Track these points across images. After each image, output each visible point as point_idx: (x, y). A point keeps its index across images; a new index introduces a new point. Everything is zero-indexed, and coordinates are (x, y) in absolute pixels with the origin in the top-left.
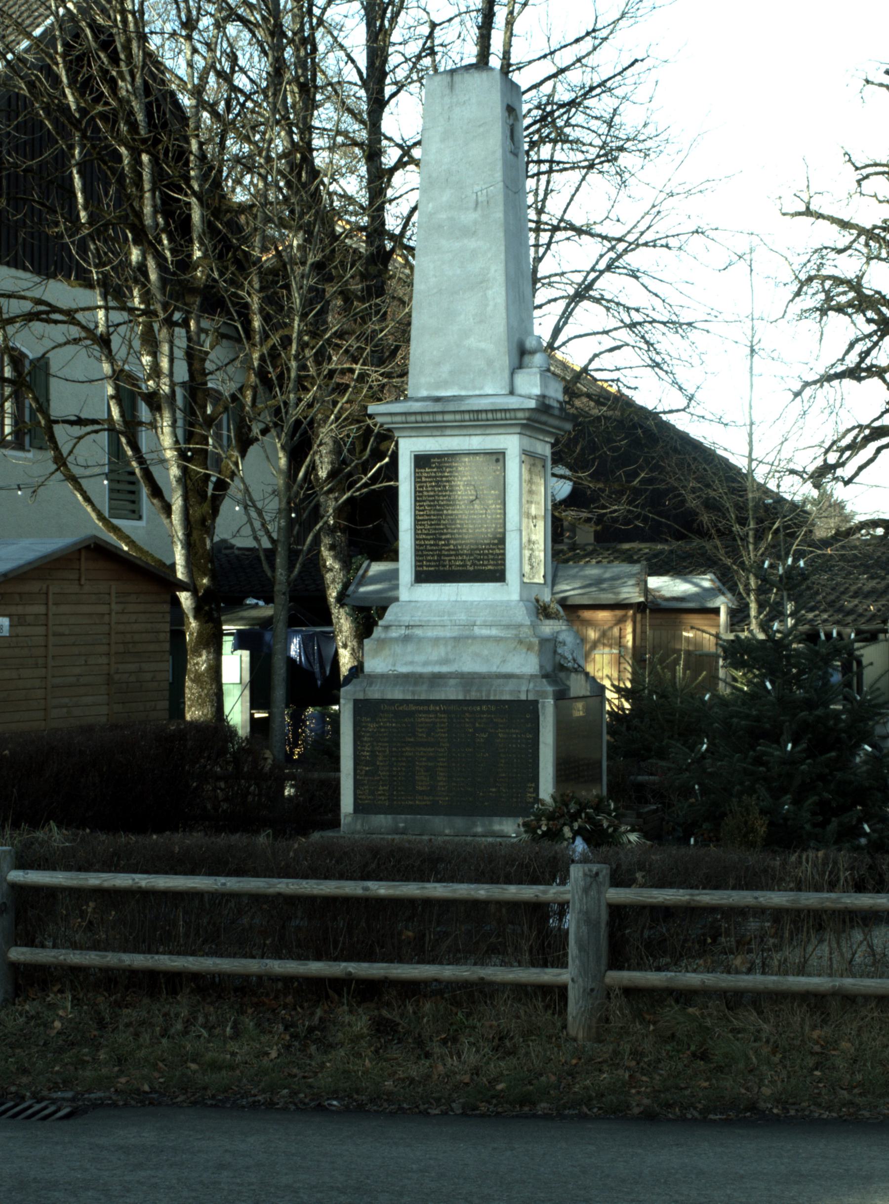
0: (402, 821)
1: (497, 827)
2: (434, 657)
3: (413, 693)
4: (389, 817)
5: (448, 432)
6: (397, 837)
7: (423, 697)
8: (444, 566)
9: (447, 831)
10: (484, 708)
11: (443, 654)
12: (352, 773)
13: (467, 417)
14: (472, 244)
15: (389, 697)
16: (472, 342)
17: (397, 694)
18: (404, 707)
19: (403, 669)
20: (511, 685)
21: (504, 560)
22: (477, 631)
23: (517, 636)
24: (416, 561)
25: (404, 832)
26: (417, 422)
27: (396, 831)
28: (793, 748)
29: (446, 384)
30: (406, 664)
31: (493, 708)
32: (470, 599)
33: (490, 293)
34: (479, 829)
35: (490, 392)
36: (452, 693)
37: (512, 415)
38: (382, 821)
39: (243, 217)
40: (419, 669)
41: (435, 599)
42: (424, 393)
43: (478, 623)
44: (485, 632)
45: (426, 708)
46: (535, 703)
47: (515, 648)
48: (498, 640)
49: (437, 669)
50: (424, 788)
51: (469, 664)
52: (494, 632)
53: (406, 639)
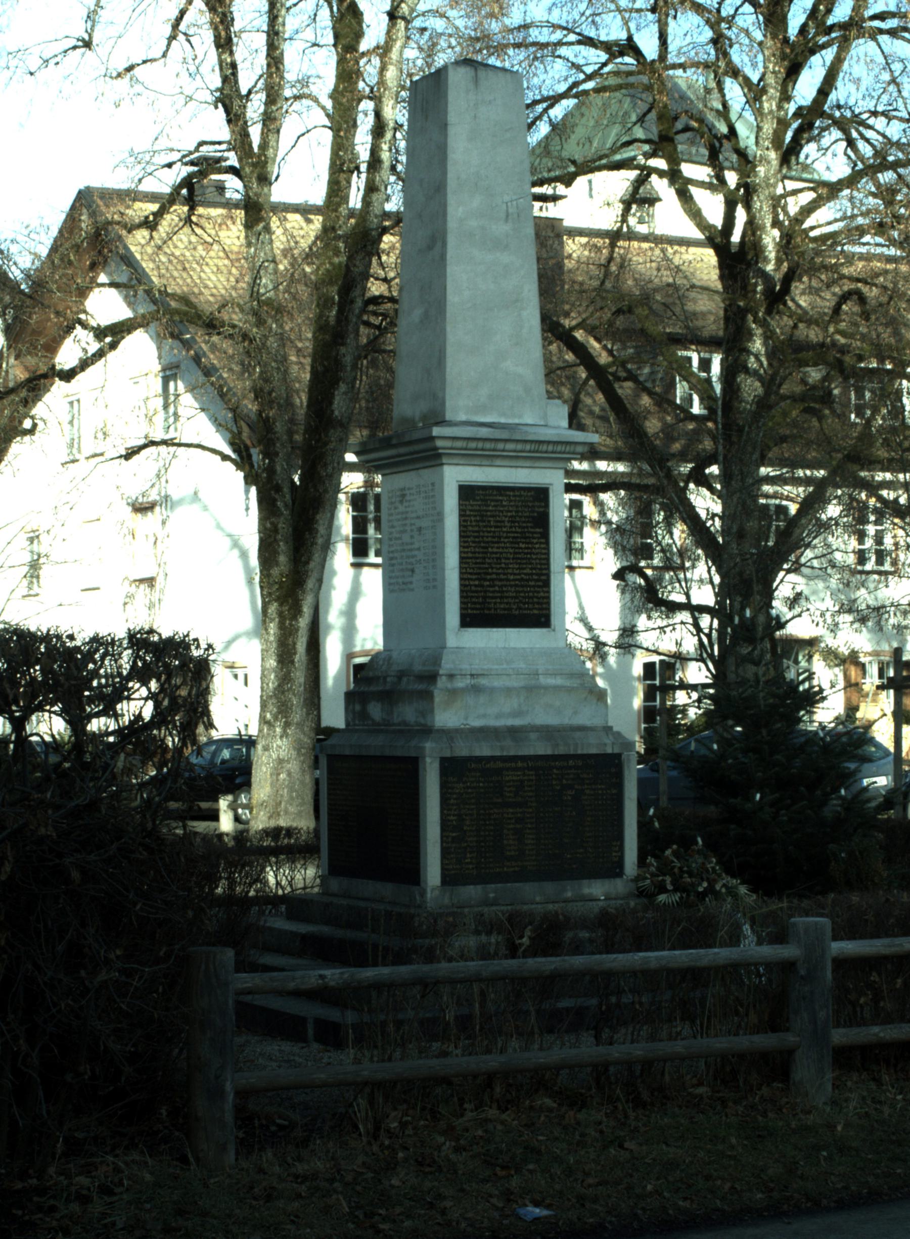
0: (492, 890)
1: (586, 891)
4: (479, 887)
5: (498, 462)
6: (486, 909)
7: (512, 753)
8: (489, 609)
9: (538, 899)
10: (571, 763)
11: (516, 705)
13: (528, 447)
14: (505, 258)
15: (477, 753)
16: (508, 365)
17: (484, 750)
18: (491, 765)
19: (477, 723)
21: (549, 603)
22: (544, 681)
23: (582, 685)
24: (461, 603)
25: (495, 903)
26: (482, 450)
27: (486, 903)
28: (761, 798)
29: (483, 409)
30: (479, 717)
31: (580, 763)
32: (518, 645)
33: (524, 314)
35: (530, 421)
36: (541, 748)
37: (572, 448)
38: (471, 892)
39: (391, 206)
40: (492, 723)
41: (483, 645)
42: (463, 417)
43: (540, 672)
44: (551, 681)
45: (513, 765)
46: (619, 756)
47: (586, 699)
48: (569, 690)
49: (510, 722)
50: (513, 853)
51: (542, 717)
52: (559, 681)
53: (476, 690)
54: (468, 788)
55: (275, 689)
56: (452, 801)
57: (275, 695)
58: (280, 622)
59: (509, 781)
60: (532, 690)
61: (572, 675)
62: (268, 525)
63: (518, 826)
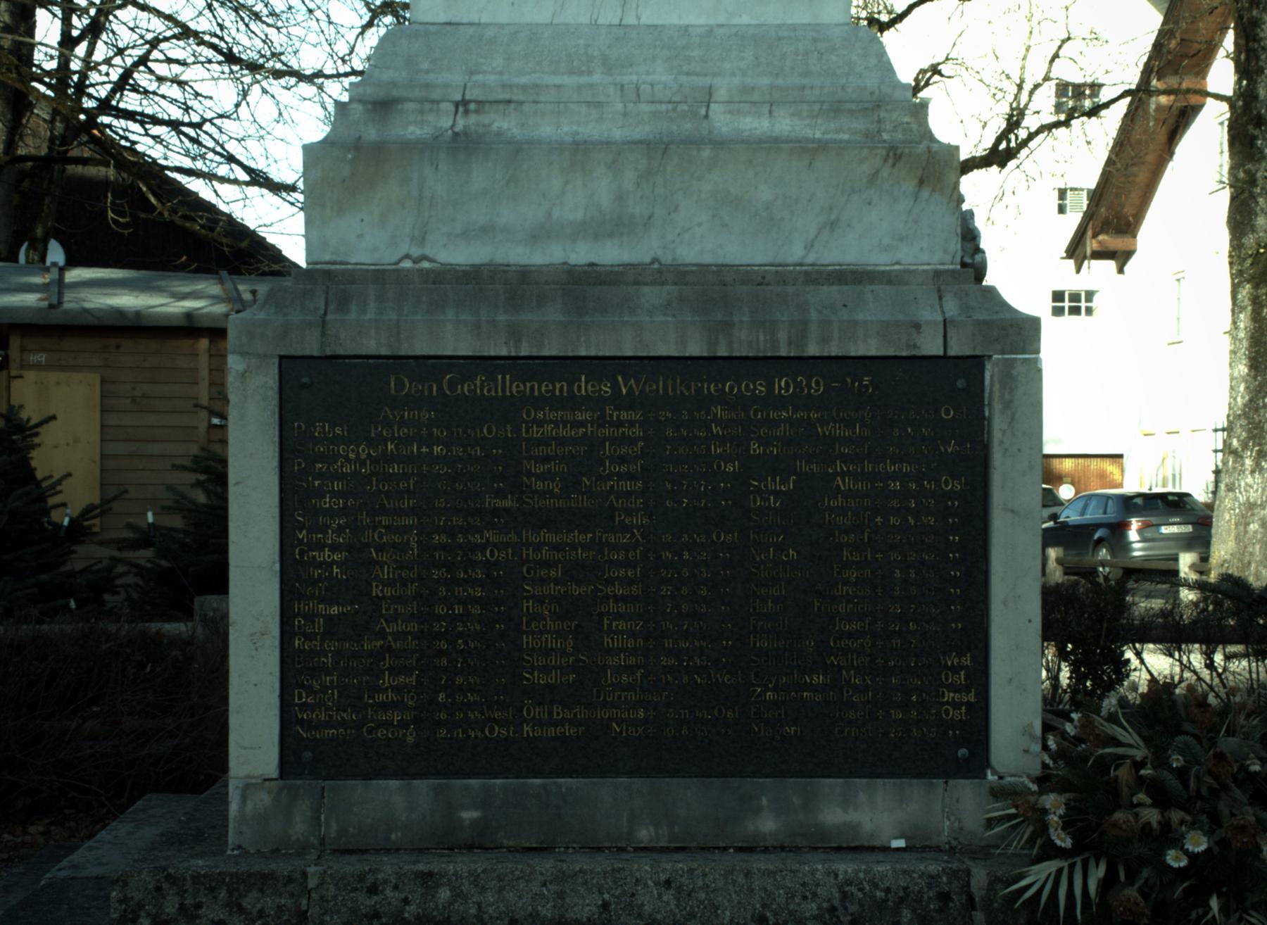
1: (832, 816)
2: (572, 209)
3: (515, 333)
4: (422, 786)
9: (644, 834)
11: (605, 198)
12: (275, 629)
15: (422, 347)
17: (453, 338)
18: (479, 385)
19: (459, 255)
20: (874, 305)
22: (722, 121)
23: (870, 138)
31: (816, 388)
34: (767, 825)
36: (665, 334)
40: (518, 254)
41: (544, 17)
44: (755, 124)
45: (560, 387)
49: (582, 254)
51: (702, 235)
52: (784, 124)
53: (463, 146)
54: (388, 458)
55: (1245, 405)
56: (327, 502)
57: (1245, 415)
58: (1253, 310)
59: (544, 442)
60: (674, 148)
61: (834, 108)
62: (1241, 175)
63: (576, 590)
